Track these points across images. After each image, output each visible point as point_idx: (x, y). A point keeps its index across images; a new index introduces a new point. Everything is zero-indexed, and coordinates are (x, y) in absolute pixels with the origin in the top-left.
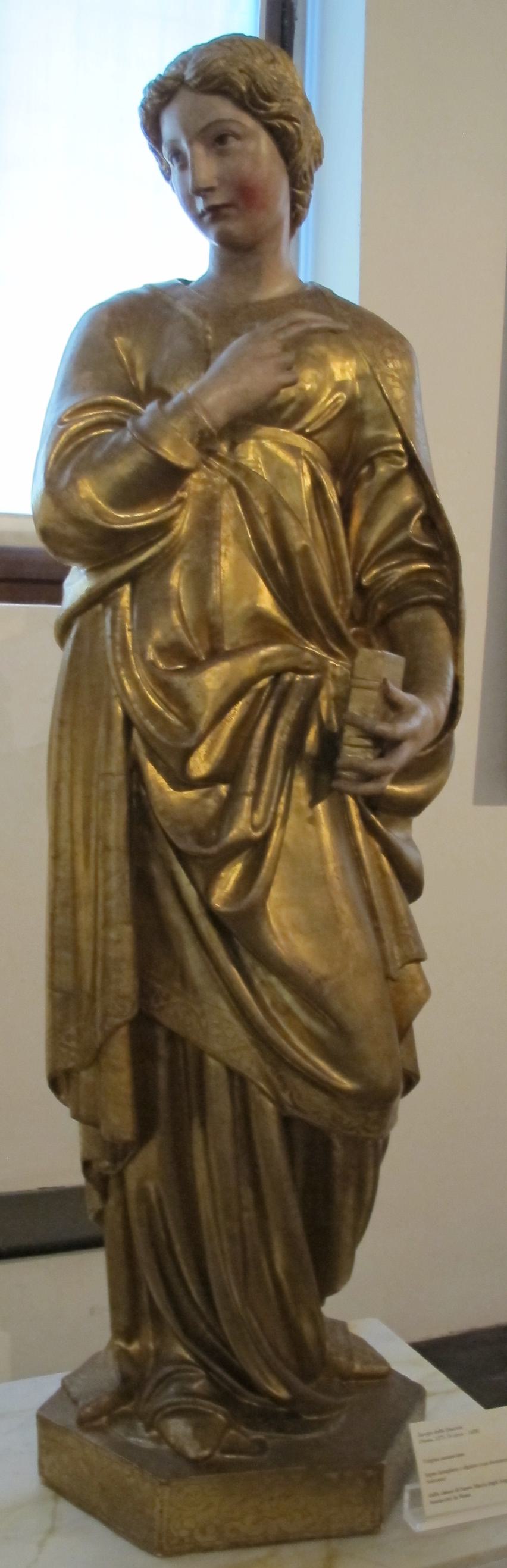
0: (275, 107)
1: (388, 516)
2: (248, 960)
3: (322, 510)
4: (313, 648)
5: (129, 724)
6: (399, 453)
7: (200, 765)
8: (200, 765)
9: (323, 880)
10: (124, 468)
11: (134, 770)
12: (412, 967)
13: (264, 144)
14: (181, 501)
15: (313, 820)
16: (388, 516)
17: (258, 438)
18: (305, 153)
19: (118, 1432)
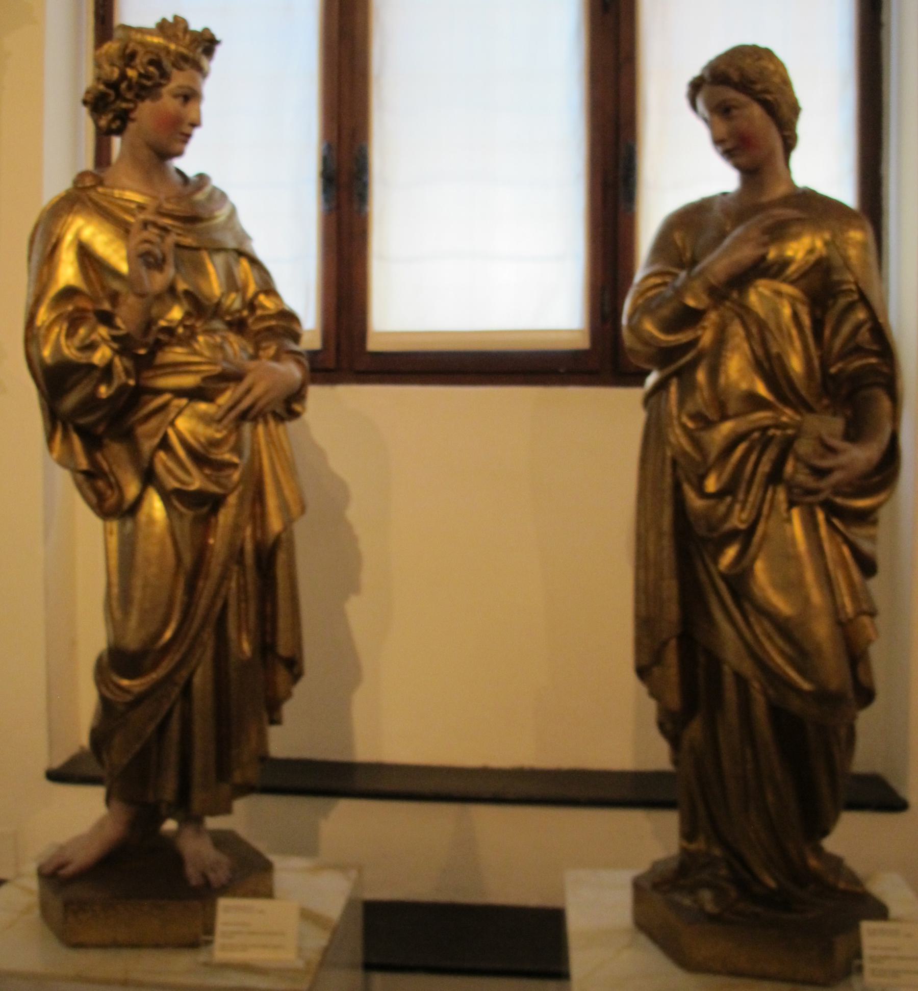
0: (759, 87)
1: (846, 329)
2: (747, 606)
3: (181, 369)
4: (789, 411)
5: (674, 463)
6: (851, 290)
7: (711, 484)
8: (711, 484)
9: (796, 558)
10: (665, 312)
11: (677, 488)
12: (865, 620)
13: (756, 111)
14: (704, 328)
15: (789, 520)
16: (846, 329)
17: (756, 287)
18: (785, 110)
19: (677, 897)
